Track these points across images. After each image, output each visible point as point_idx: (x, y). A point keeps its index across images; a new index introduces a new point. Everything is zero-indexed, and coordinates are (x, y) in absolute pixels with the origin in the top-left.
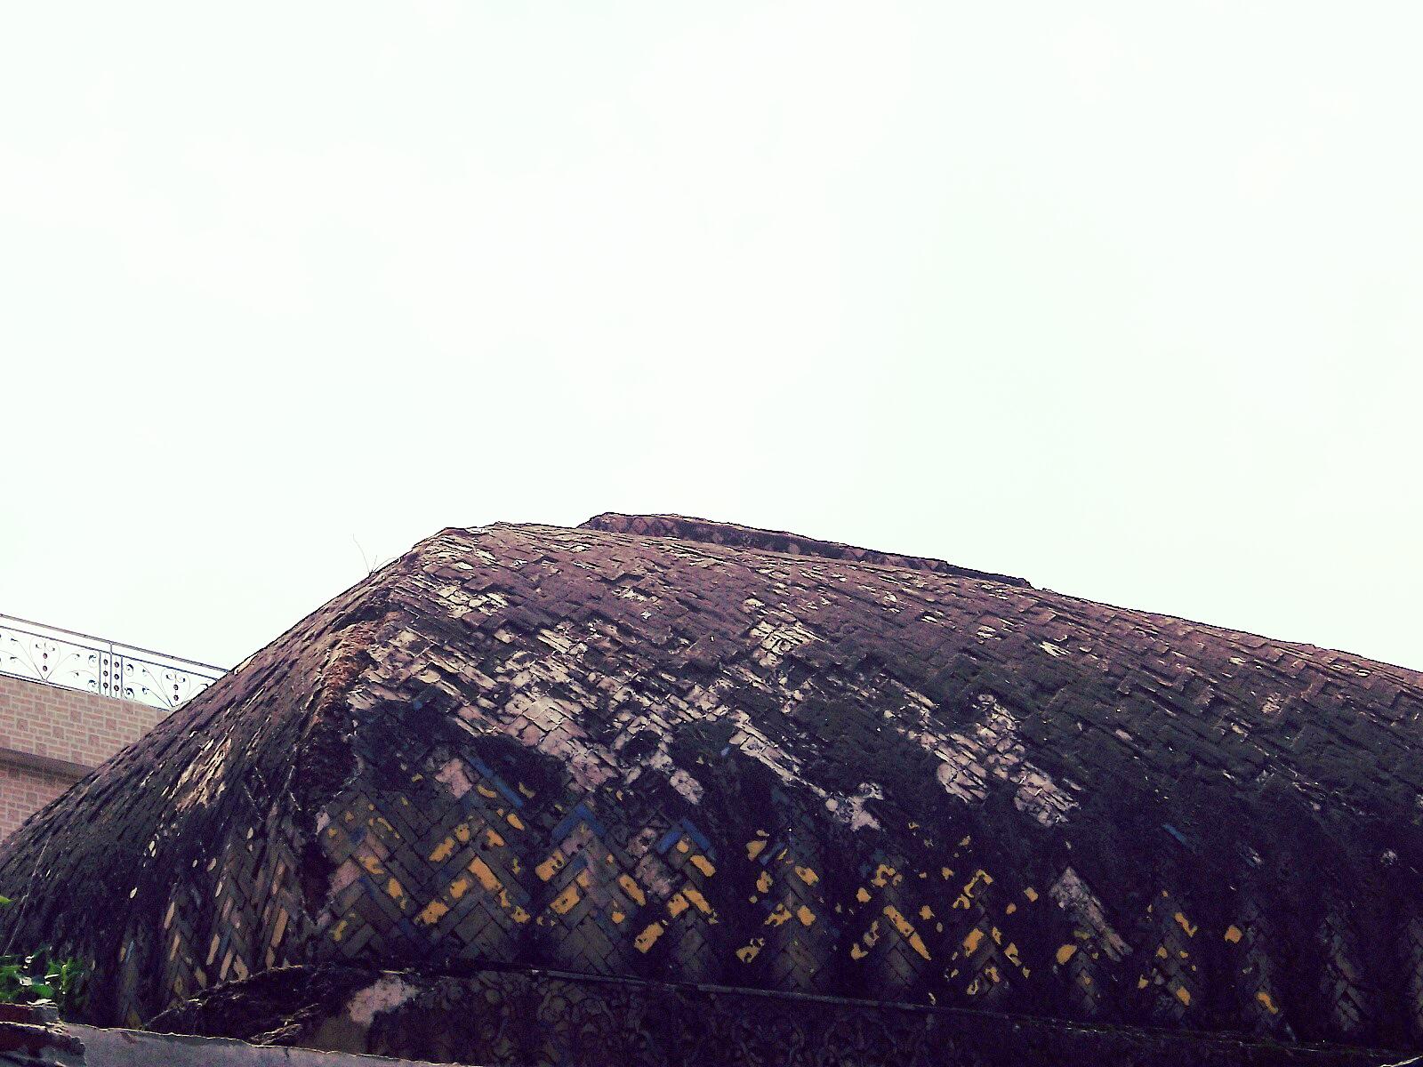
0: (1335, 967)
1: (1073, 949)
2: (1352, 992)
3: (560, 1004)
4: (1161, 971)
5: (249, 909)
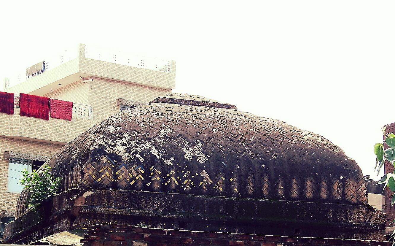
4: (218, 186)
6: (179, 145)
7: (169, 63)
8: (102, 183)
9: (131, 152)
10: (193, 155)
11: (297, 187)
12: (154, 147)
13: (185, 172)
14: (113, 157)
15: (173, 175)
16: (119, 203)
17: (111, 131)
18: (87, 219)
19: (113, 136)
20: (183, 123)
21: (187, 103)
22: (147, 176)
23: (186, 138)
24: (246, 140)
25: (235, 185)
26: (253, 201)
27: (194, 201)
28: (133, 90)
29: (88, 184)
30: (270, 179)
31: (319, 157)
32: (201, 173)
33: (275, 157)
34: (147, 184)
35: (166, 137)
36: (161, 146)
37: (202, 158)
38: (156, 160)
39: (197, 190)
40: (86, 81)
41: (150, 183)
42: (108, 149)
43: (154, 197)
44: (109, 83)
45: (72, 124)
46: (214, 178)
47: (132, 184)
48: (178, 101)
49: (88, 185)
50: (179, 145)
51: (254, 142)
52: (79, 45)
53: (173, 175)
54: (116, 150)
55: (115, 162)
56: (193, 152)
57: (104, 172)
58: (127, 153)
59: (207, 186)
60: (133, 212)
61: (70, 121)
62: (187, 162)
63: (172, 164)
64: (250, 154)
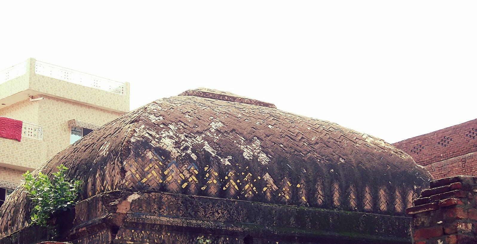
2: (321, 197)
3: (166, 199)
4: (284, 193)
6: (235, 141)
7: (123, 85)
8: (148, 184)
9: (180, 147)
10: (252, 154)
11: (370, 197)
12: (206, 142)
13: (246, 174)
14: (160, 152)
15: (232, 178)
16: (172, 211)
17: (153, 121)
18: (133, 231)
19: (155, 126)
20: (233, 117)
21: (221, 98)
22: (202, 177)
23: (241, 134)
24: (308, 140)
25: (303, 192)
26: (328, 212)
27: (260, 211)
28: (85, 112)
29: (130, 186)
30: (340, 186)
31: (388, 163)
32: (264, 177)
33: (343, 161)
34: (202, 188)
35: (218, 131)
36: (214, 141)
37: (263, 158)
38: (211, 158)
39: (260, 197)
40: (35, 100)
41: (205, 187)
42: (153, 142)
43: (213, 203)
44: (60, 103)
45: (22, 144)
46: (279, 183)
47: (184, 187)
48: (211, 95)
49: (130, 187)
50: (235, 141)
51: (317, 143)
52: (30, 59)
53: (232, 178)
54: (163, 144)
55: (162, 159)
56: (252, 151)
57: (150, 170)
58: (176, 147)
59: (271, 193)
61: (20, 141)
62: (246, 163)
63: (230, 164)
64: (315, 156)
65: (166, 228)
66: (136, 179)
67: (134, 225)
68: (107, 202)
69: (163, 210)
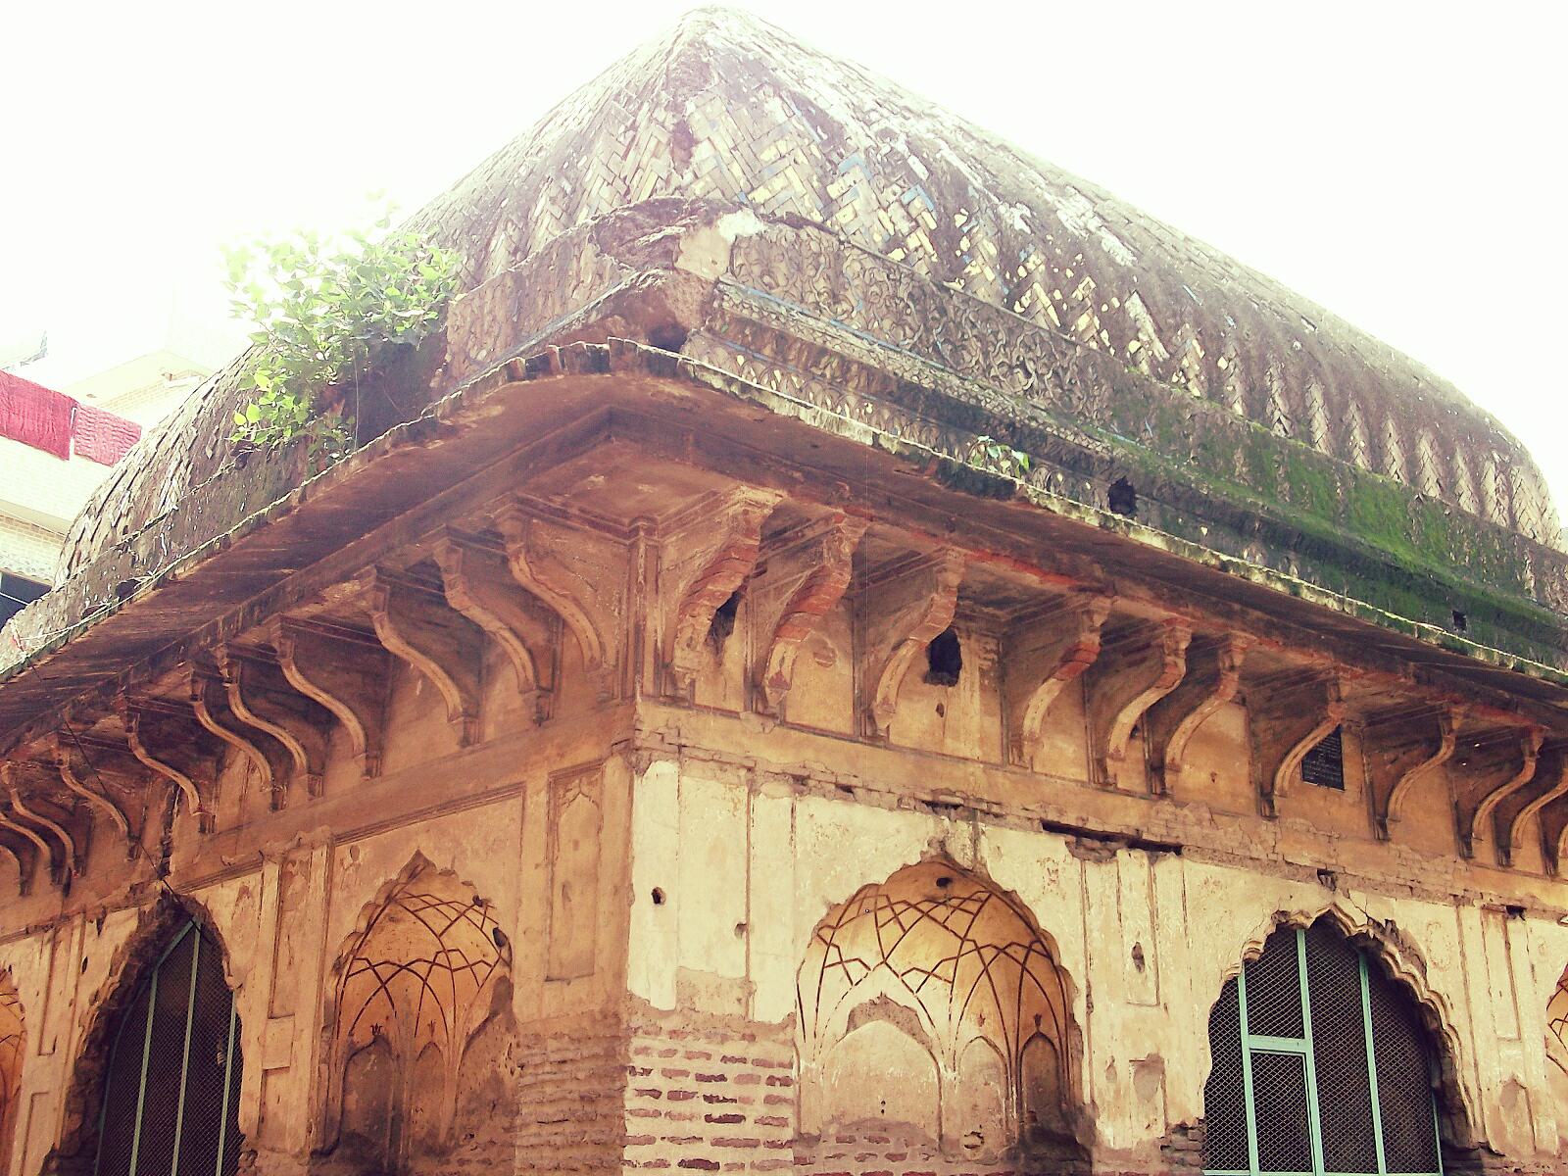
0: (1274, 402)
1: (1138, 345)
2: (1283, 419)
3: (857, 267)
4: (1184, 375)
5: (619, 183)
18: (741, 359)
60: (941, 378)
65: (862, 380)
66: (732, 181)
67: (747, 332)
68: (621, 239)
69: (845, 306)
